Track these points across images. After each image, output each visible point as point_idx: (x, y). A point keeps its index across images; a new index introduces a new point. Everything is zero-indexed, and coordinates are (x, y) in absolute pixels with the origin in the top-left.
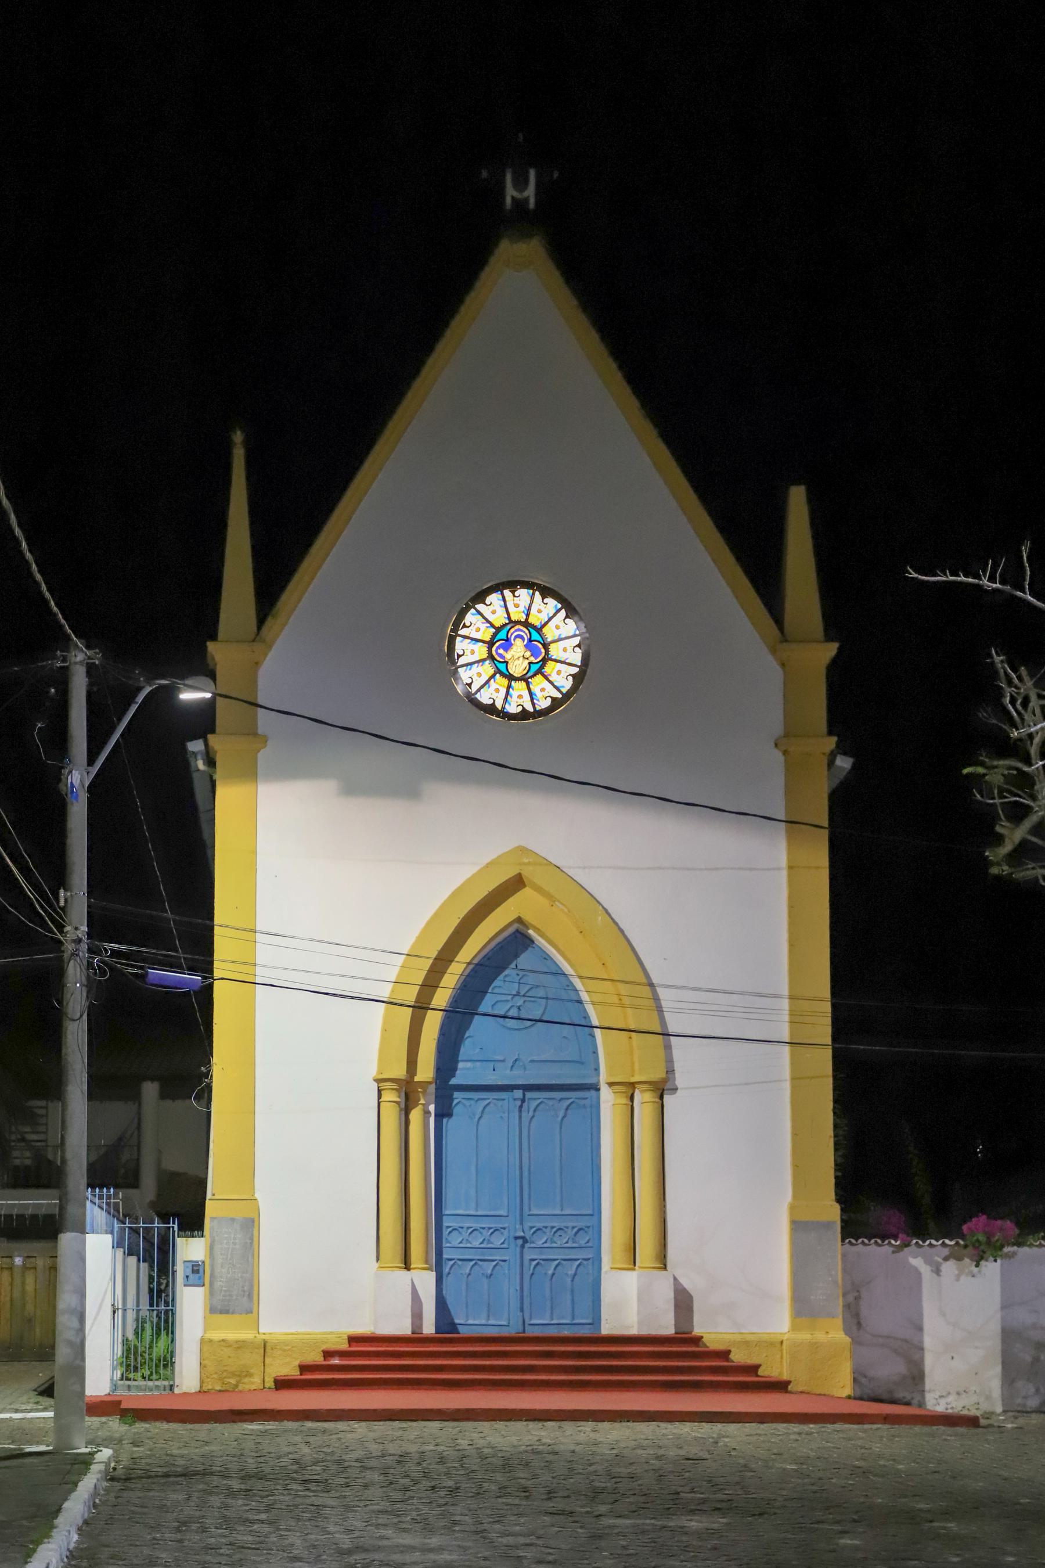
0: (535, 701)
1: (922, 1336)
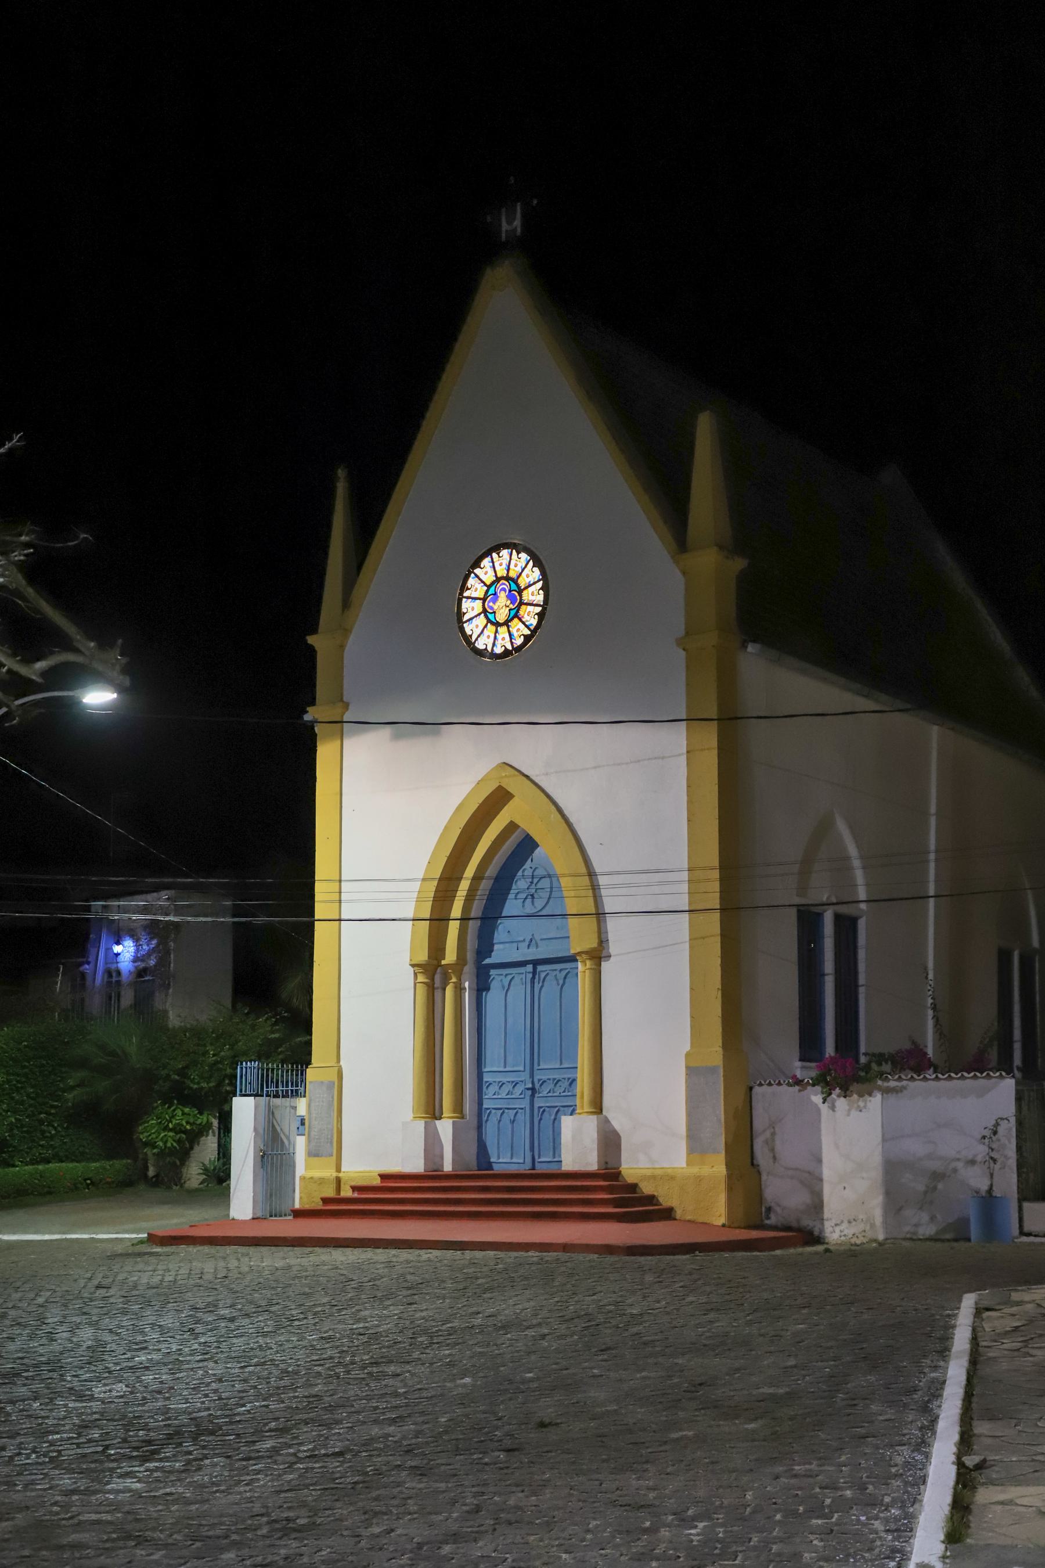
0: (513, 641)
1: (821, 1166)
